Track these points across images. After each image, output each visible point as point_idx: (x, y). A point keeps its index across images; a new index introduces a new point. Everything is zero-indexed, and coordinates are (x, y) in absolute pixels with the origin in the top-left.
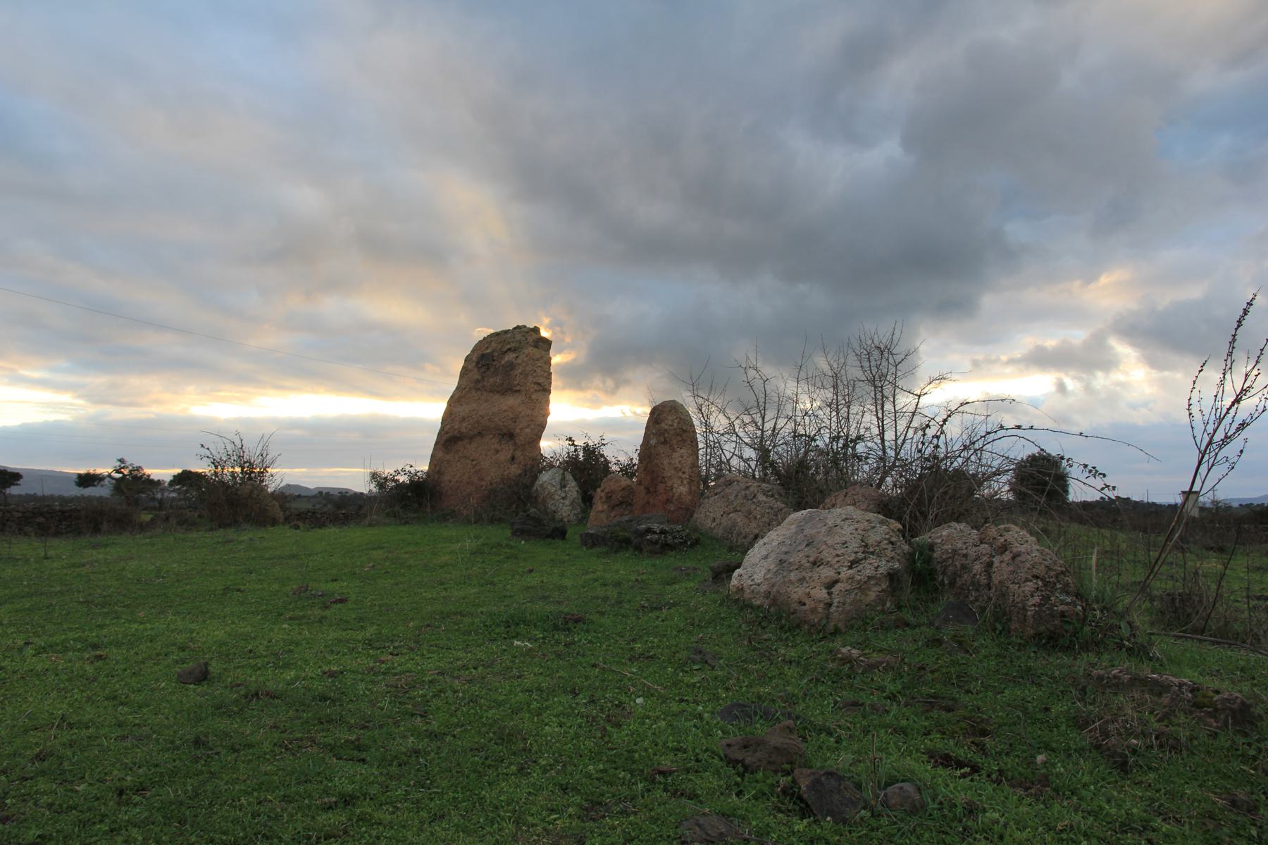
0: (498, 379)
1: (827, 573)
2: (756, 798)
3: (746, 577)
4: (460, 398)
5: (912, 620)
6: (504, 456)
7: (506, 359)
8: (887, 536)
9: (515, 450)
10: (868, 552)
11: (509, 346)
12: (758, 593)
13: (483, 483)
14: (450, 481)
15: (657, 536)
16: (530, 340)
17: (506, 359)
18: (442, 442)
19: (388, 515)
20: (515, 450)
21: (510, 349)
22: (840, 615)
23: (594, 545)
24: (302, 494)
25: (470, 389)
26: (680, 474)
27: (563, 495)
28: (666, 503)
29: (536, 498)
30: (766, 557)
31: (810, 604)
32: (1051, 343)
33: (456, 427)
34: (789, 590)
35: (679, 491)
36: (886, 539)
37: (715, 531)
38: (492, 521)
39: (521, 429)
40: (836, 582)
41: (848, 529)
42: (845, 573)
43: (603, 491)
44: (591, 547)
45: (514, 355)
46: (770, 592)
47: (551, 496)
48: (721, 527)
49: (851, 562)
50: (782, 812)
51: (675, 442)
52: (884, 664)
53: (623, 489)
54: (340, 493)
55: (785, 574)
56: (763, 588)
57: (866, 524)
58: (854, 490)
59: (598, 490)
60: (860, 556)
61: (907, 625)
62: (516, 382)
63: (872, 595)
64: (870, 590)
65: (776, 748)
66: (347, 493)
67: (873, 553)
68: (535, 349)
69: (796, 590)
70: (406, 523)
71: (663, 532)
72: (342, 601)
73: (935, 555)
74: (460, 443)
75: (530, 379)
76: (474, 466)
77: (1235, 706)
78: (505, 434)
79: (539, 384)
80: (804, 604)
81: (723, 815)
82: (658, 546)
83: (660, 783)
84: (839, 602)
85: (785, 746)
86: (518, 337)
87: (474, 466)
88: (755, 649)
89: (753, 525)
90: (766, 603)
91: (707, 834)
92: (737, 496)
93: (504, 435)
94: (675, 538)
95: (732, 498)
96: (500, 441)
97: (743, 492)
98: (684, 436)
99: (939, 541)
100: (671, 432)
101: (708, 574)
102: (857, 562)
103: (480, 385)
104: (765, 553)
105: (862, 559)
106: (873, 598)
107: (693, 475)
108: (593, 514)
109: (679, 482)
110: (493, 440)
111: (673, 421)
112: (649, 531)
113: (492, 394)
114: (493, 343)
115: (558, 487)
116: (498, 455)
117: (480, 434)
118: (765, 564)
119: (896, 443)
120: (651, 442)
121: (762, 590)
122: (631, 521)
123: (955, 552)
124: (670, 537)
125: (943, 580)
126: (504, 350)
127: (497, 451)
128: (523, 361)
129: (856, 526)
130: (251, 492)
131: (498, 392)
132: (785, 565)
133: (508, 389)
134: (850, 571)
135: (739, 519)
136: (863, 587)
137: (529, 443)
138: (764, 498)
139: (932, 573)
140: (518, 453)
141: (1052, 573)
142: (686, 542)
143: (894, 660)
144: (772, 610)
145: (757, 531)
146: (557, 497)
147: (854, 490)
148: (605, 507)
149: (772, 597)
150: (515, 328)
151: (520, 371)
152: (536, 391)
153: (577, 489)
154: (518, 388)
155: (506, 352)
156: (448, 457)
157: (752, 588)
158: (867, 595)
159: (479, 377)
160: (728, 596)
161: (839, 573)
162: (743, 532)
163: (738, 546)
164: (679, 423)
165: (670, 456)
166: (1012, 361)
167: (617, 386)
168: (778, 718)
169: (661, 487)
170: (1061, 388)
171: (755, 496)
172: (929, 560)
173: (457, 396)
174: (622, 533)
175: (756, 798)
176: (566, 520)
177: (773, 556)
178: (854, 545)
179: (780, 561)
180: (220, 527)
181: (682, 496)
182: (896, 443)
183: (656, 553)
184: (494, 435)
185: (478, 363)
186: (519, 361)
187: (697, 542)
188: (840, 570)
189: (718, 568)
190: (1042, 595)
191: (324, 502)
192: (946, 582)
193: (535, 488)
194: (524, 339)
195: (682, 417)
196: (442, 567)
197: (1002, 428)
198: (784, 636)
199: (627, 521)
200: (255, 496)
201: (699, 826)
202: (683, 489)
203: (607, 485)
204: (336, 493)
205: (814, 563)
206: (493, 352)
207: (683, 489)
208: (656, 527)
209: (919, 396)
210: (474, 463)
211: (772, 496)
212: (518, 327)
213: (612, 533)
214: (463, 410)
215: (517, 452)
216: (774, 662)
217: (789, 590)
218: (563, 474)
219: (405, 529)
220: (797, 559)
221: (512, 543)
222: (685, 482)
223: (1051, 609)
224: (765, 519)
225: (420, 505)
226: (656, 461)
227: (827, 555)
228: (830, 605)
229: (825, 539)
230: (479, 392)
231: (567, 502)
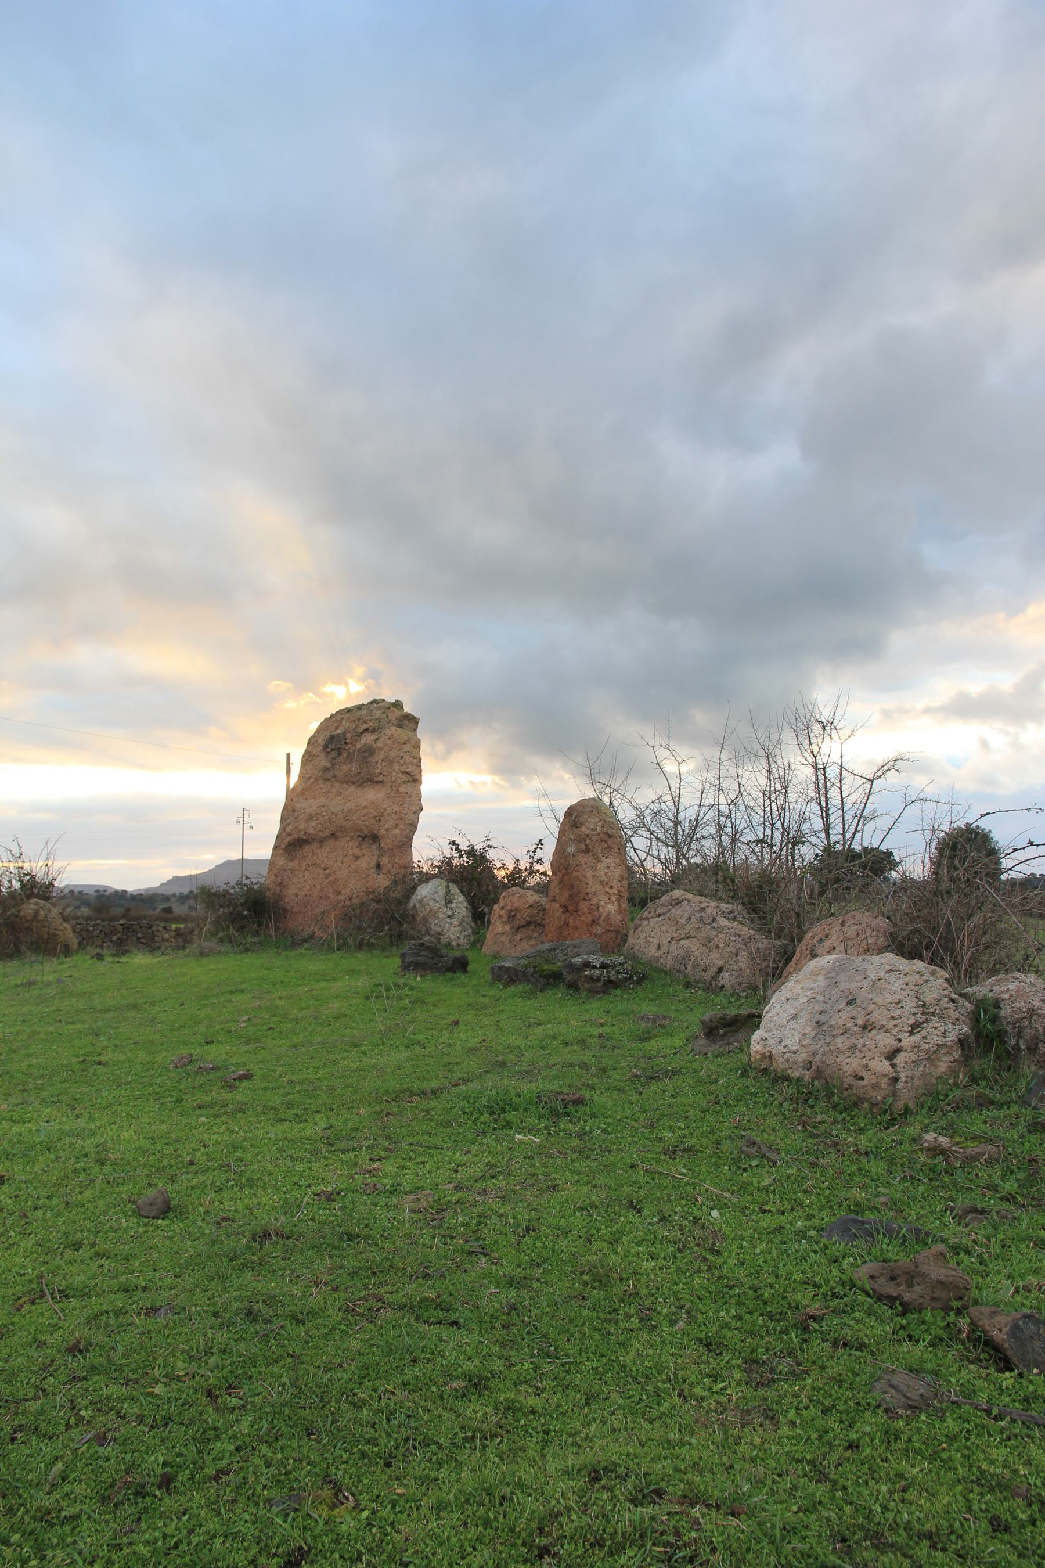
0: (354, 767)
1: (886, 1041)
2: (932, 1345)
3: (772, 1041)
5: (995, 1095)
6: (367, 862)
7: (363, 742)
10: (928, 1014)
11: (365, 726)
12: (795, 1062)
13: (341, 897)
14: (297, 895)
15: (597, 972)
18: (283, 846)
19: (221, 940)
21: (367, 730)
23: (511, 981)
25: (317, 779)
26: (607, 889)
27: (449, 913)
28: (591, 925)
29: (413, 916)
30: (795, 1017)
31: (869, 1079)
32: (975, 688)
33: (302, 827)
34: (839, 1060)
36: (945, 996)
37: (661, 960)
38: (360, 946)
39: (387, 830)
40: (898, 1051)
41: (897, 984)
43: (503, 908)
44: (506, 985)
45: (373, 737)
46: (810, 1062)
47: (434, 913)
48: (669, 957)
49: (911, 1026)
50: (972, 1362)
52: (986, 1156)
53: (531, 906)
54: (97, 891)
55: (828, 1040)
56: (802, 1057)
57: (917, 976)
58: (854, 917)
59: (496, 906)
60: (920, 1018)
61: (992, 1102)
62: (377, 771)
63: (943, 1066)
64: (940, 1061)
65: (940, 1282)
66: (105, 891)
67: (933, 1014)
68: (400, 730)
69: (848, 1060)
70: (247, 950)
71: (604, 966)
72: (247, 1077)
73: (1003, 1013)
74: (307, 847)
75: (396, 767)
76: (327, 876)
78: (366, 836)
79: (408, 773)
80: (862, 1078)
81: (911, 1371)
82: (599, 984)
83: (816, 1331)
85: (951, 1279)
86: (377, 714)
87: (327, 876)
88: (812, 1136)
89: (715, 955)
90: (808, 1076)
91: (905, 1396)
92: (690, 919)
94: (618, 973)
95: (683, 921)
96: (360, 845)
97: (698, 915)
99: (1007, 996)
101: (697, 1029)
102: (918, 1026)
103: (329, 775)
104: (792, 1012)
105: (923, 1022)
106: (943, 1070)
108: (489, 935)
109: (606, 899)
110: (351, 844)
111: (596, 824)
112: (587, 965)
113: (345, 786)
114: (344, 722)
115: (443, 903)
117: (333, 835)
118: (797, 1026)
119: (844, 837)
120: (569, 850)
121: (800, 1060)
122: (555, 949)
123: (1032, 1012)
124: (613, 972)
125: (1018, 1044)
127: (357, 858)
129: (906, 979)
130: (37, 912)
131: (354, 783)
132: (825, 1027)
134: (912, 1038)
135: (694, 946)
136: (931, 1057)
137: (399, 847)
138: (725, 922)
139: (1001, 1035)
140: (385, 860)
142: (631, 977)
143: (995, 1149)
144: (816, 1083)
145: (720, 963)
146: (441, 916)
147: (854, 917)
148: (507, 928)
149: (814, 1067)
150: (371, 703)
151: (381, 757)
153: (465, 904)
154: (380, 778)
155: (362, 733)
156: (291, 865)
157: (785, 1056)
158: (936, 1067)
159: (328, 765)
160: (749, 1064)
161: (900, 1040)
162: (701, 963)
163: (697, 982)
164: (603, 826)
166: (927, 711)
167: (449, 752)
168: (904, 1236)
169: (584, 906)
170: (984, 744)
171: (714, 920)
172: (995, 1019)
174: (546, 967)
175: (932, 1345)
176: (454, 943)
177: (805, 1015)
178: (910, 1005)
179: (817, 1022)
181: (611, 916)
182: (844, 837)
183: (597, 992)
184: (352, 837)
185: (325, 746)
186: (379, 744)
187: (643, 978)
189: (711, 1021)
191: (77, 903)
192: (1023, 1047)
193: (411, 905)
194: (384, 716)
195: (607, 819)
196: (337, 1018)
197: (1031, 843)
198: (840, 1118)
199: (550, 950)
200: (41, 918)
201: (892, 1386)
202: (612, 908)
203: (510, 899)
204: (92, 892)
205: (864, 1027)
206: (345, 733)
208: (596, 960)
209: (872, 781)
210: (327, 871)
211: (734, 919)
212: (374, 702)
213: (534, 967)
214: (309, 805)
216: (846, 1153)
217: (839, 1060)
218: (448, 887)
219: (249, 959)
220: (841, 1022)
221: (401, 981)
224: (730, 949)
225: (260, 925)
226: (575, 874)
227: (879, 1016)
228: (896, 1080)
229: (870, 996)
230: (329, 783)
231: (455, 921)
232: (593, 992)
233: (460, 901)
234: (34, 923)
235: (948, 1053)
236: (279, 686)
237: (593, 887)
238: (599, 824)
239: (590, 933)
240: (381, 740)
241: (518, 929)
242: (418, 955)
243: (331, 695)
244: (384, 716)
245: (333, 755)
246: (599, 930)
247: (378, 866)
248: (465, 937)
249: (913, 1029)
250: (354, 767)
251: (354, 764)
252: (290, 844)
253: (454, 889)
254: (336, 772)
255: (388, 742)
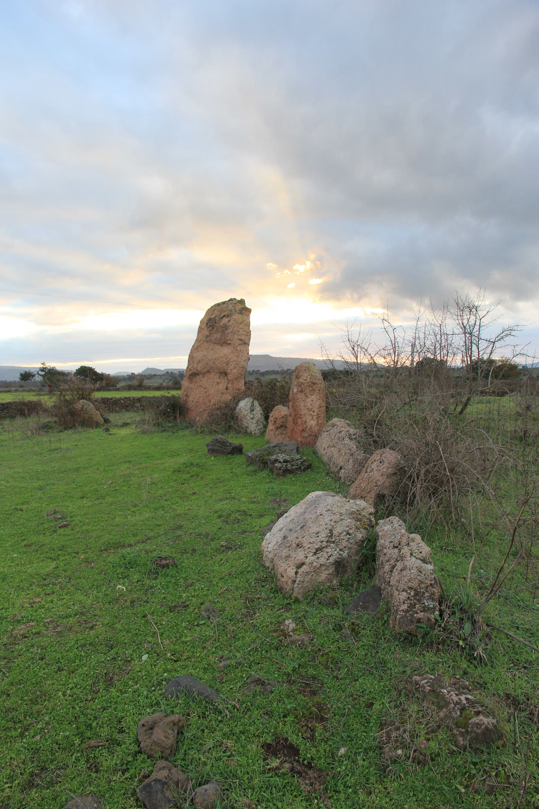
0: (218, 335)
1: (300, 555)
4: (197, 348)
6: (222, 386)
8: (348, 529)
9: (228, 383)
11: (224, 314)
14: (193, 401)
16: (237, 308)
17: (223, 322)
20: (228, 383)
21: (225, 316)
22: (299, 590)
24: (157, 374)
25: (203, 341)
26: (311, 413)
27: (252, 416)
33: (195, 367)
35: (310, 424)
36: (346, 531)
39: (231, 370)
42: (311, 558)
45: (228, 320)
51: (308, 391)
52: (300, 642)
53: (283, 417)
62: (228, 338)
63: (324, 576)
64: (322, 573)
76: (206, 392)
77: (479, 731)
78: (222, 373)
79: (241, 340)
80: (283, 577)
84: (300, 581)
85: (159, 741)
86: (230, 307)
87: (206, 392)
93: (221, 373)
94: (293, 465)
96: (220, 377)
97: (338, 435)
98: (314, 387)
100: (306, 385)
103: (208, 339)
106: (323, 578)
107: (320, 413)
109: (311, 418)
110: (216, 376)
111: (307, 377)
112: (276, 461)
115: (249, 411)
116: (218, 386)
126: (222, 316)
127: (218, 383)
128: (233, 324)
130: (83, 406)
131: (219, 344)
133: (224, 343)
136: (317, 570)
137: (236, 379)
140: (230, 385)
141: (423, 585)
142: (300, 467)
146: (248, 418)
150: (229, 300)
151: (231, 330)
152: (239, 344)
153: (260, 412)
154: (229, 342)
156: (191, 386)
159: (208, 334)
165: (305, 401)
167: (360, 298)
169: (299, 421)
173: (196, 346)
178: (323, 535)
180: (65, 429)
185: (207, 324)
186: (230, 324)
188: (308, 555)
190: (411, 604)
191: (170, 378)
195: (313, 374)
202: (313, 423)
204: (177, 372)
206: (215, 317)
207: (313, 423)
209: (494, 343)
212: (231, 300)
213: (260, 457)
214: (199, 355)
215: (229, 385)
218: (253, 402)
222: (314, 418)
223: (412, 615)
226: (297, 403)
230: (208, 343)
231: (254, 421)
232: (278, 475)
233: (258, 410)
234: (82, 412)
235: (326, 569)
236: (271, 266)
237: (304, 412)
238: (309, 377)
239: (301, 435)
240: (231, 321)
241: (277, 429)
242: (214, 445)
243: (297, 270)
244: (233, 308)
245: (210, 328)
246: (306, 435)
247: (227, 389)
248: (259, 429)
249: (316, 551)
250: (218, 335)
251: (219, 334)
252: (190, 375)
253: (256, 403)
254: (211, 338)
255: (234, 323)
